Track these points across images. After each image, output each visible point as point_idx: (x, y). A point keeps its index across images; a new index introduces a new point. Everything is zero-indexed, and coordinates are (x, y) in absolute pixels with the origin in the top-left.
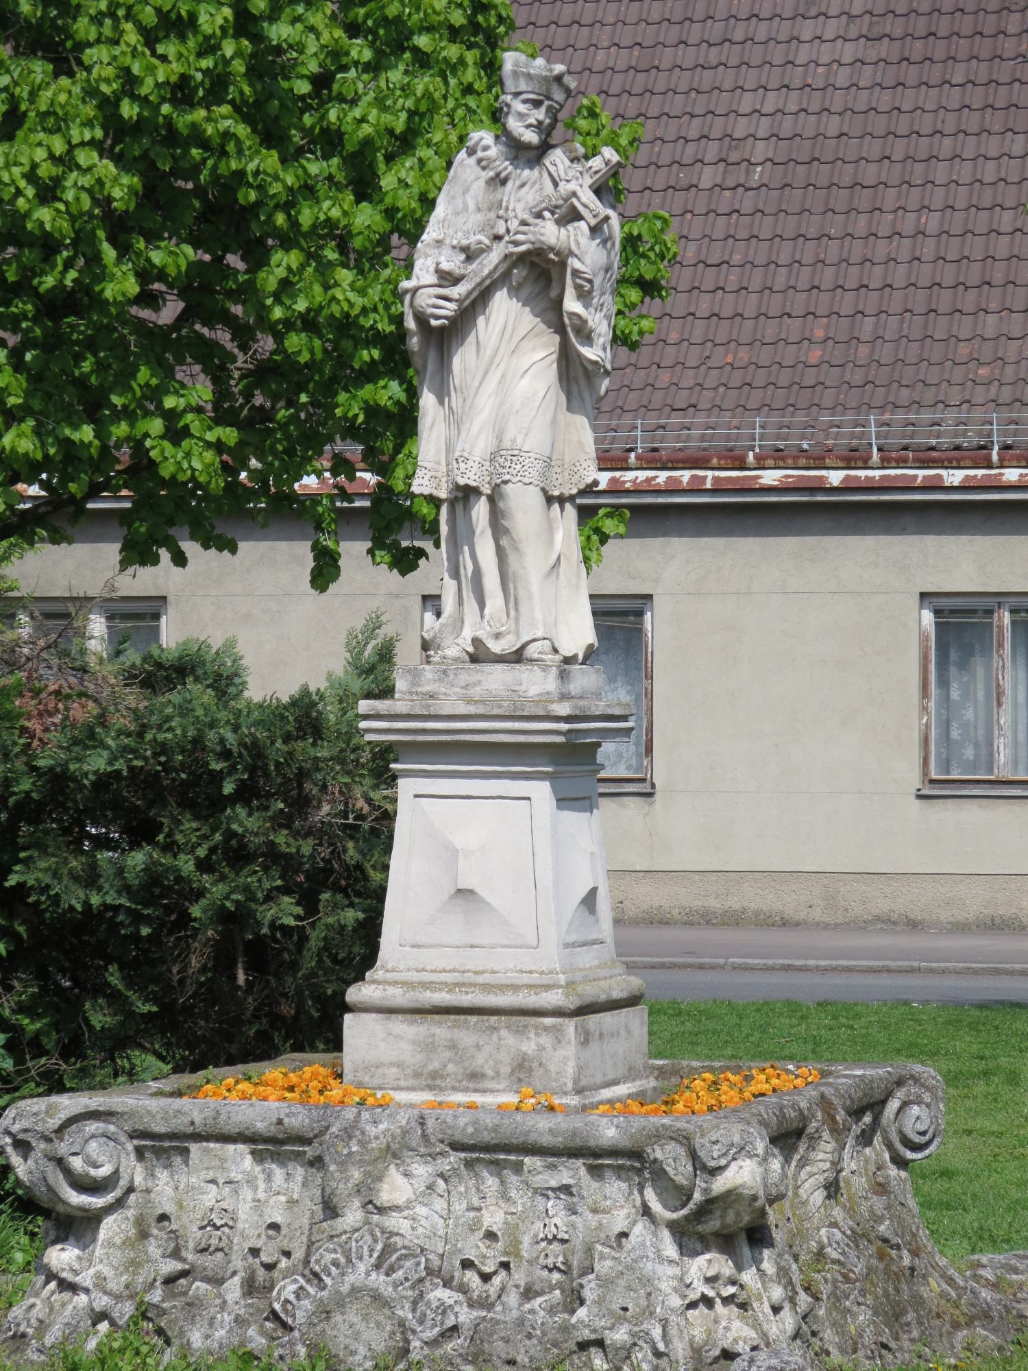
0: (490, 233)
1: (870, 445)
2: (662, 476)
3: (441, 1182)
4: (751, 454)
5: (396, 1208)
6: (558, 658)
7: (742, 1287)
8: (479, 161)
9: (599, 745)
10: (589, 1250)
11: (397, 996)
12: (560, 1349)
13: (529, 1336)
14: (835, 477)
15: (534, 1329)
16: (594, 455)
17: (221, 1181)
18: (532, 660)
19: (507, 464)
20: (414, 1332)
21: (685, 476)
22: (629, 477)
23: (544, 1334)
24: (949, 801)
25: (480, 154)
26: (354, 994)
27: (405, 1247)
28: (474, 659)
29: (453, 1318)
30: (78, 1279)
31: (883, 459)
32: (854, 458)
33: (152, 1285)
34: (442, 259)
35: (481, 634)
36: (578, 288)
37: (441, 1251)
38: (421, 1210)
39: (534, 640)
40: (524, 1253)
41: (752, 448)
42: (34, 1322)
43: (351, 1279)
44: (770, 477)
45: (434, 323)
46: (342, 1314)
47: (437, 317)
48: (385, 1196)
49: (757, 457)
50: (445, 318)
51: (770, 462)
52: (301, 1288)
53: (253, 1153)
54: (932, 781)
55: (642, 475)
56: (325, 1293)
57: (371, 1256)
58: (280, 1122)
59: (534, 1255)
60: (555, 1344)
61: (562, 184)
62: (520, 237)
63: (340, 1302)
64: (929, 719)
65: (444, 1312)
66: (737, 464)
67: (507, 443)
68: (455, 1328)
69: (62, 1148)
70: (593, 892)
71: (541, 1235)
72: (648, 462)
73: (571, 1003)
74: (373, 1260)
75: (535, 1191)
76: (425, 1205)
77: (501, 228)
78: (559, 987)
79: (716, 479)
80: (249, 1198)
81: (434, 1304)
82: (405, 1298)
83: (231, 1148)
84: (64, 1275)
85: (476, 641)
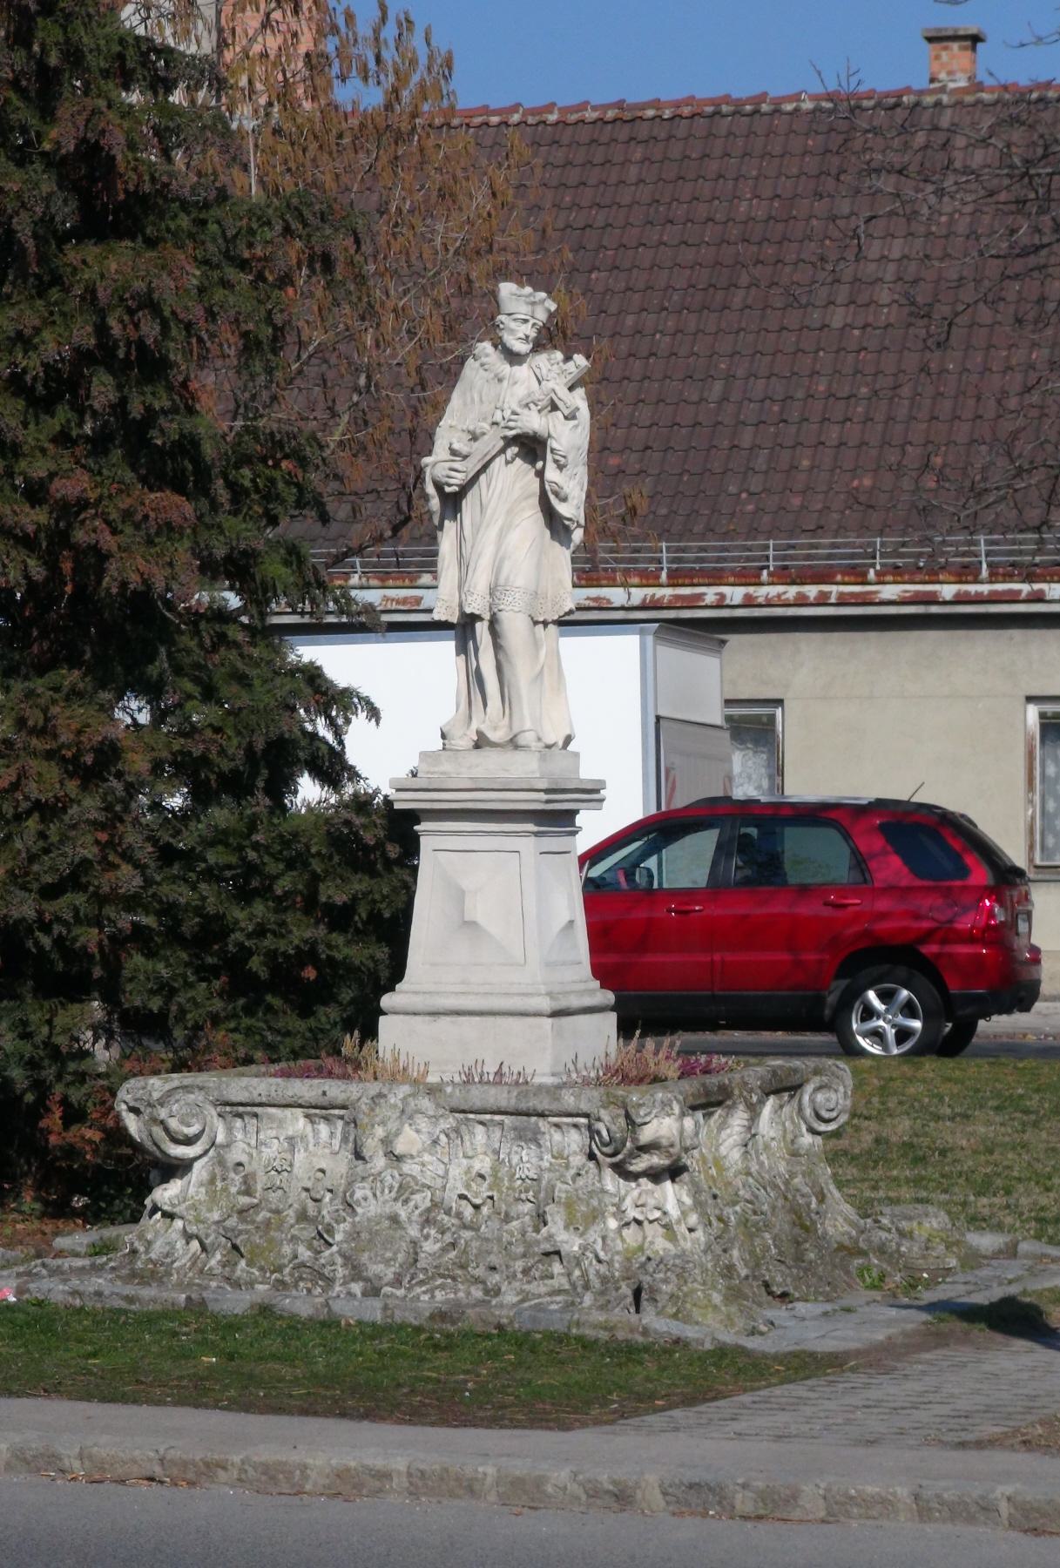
0: (490, 421)
1: (980, 563)
2: (792, 591)
4: (872, 571)
6: (541, 745)
7: (665, 1213)
8: (482, 365)
9: (576, 812)
11: (418, 1002)
21: (812, 591)
22: (762, 592)
24: (1052, 884)
26: (386, 1001)
28: (477, 746)
30: (176, 1210)
31: (991, 575)
34: (454, 440)
35: (483, 728)
41: (873, 565)
44: (890, 591)
45: (448, 489)
47: (450, 485)
48: (400, 1148)
49: (878, 574)
51: (889, 578)
53: (307, 1116)
54: (1037, 867)
55: (773, 591)
61: (543, 383)
62: (511, 424)
64: (1034, 812)
66: (860, 580)
67: (502, 581)
69: (163, 1113)
70: (571, 922)
72: (779, 577)
73: (546, 1004)
77: (498, 417)
78: (540, 995)
79: (841, 595)
83: (288, 1112)
84: (166, 1208)
85: (480, 733)
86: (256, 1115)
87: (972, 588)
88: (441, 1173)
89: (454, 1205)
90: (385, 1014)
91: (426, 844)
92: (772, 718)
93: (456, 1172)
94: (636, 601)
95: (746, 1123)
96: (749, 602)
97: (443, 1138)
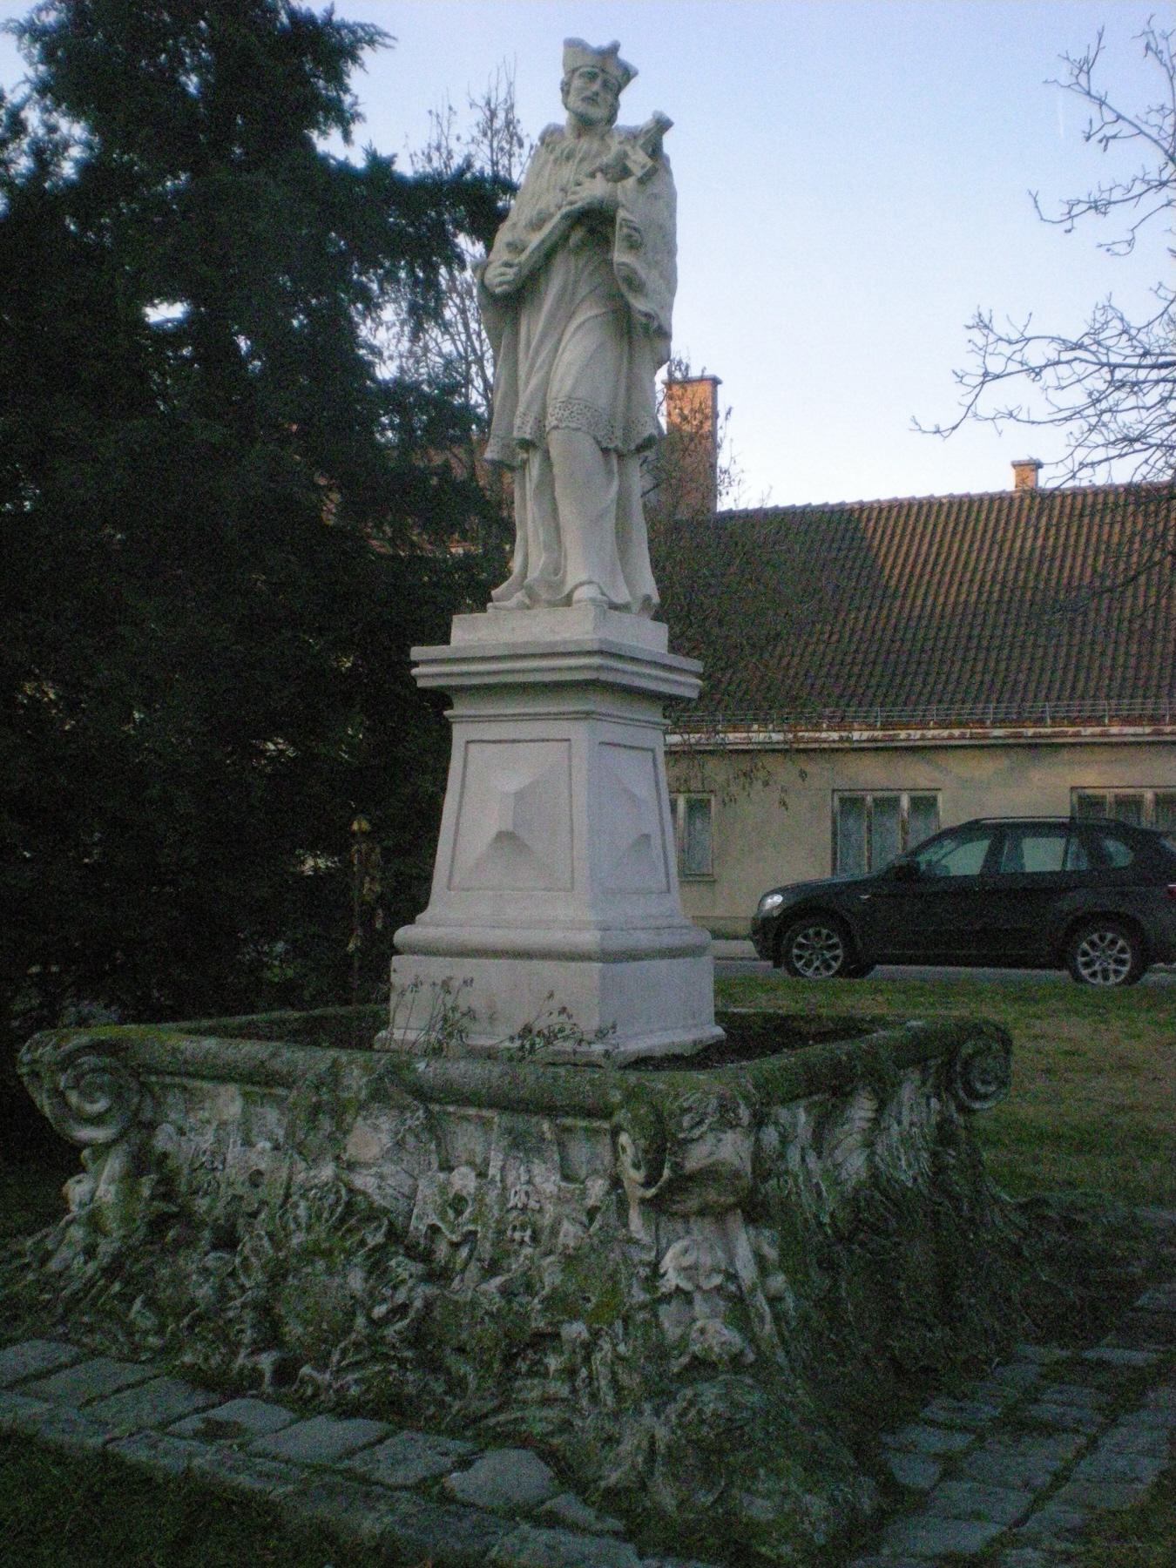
2: (945, 733)
21: (956, 732)
26: (402, 935)
55: (936, 732)
86: (185, 1089)
87: (1042, 730)
88: (406, 1190)
89: (422, 1241)
90: (398, 952)
91: (459, 734)
92: (935, 799)
93: (426, 1190)
94: (864, 738)
95: (870, 1115)
96: (923, 738)
97: (411, 1140)
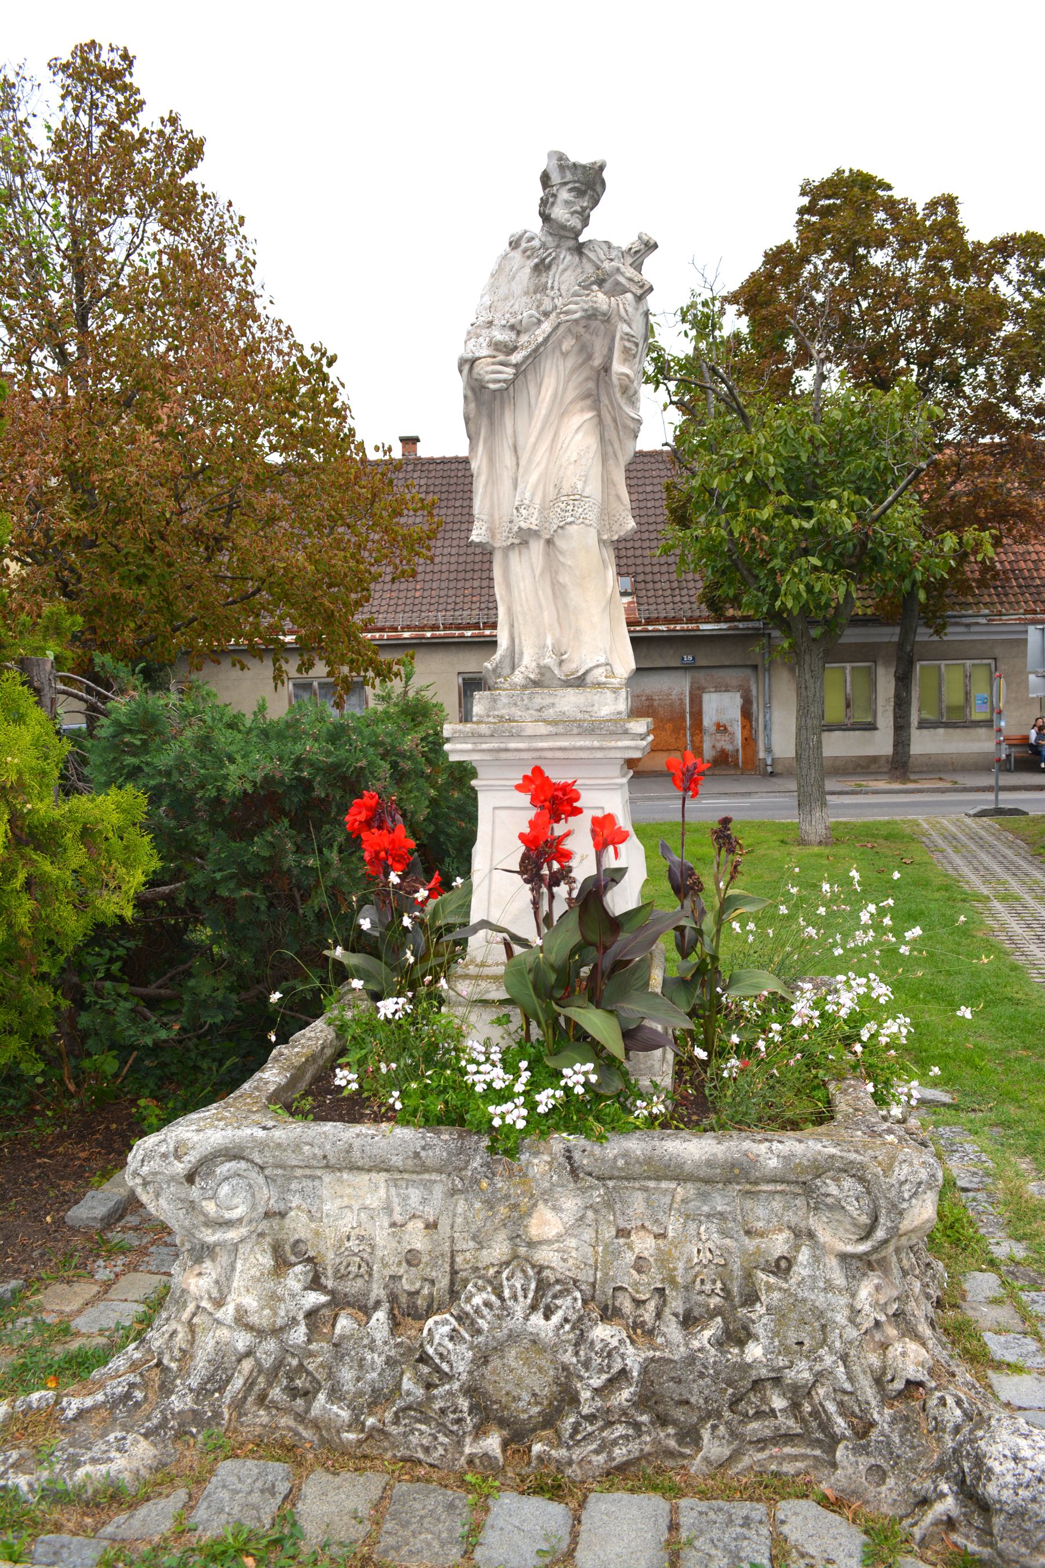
3: (590, 1214)
5: (548, 1242)
10: (748, 1276)
12: (735, 1388)
13: (702, 1375)
14: (429, 634)
15: (706, 1368)
16: (629, 507)
17: (356, 1207)
18: (599, 685)
19: (570, 508)
20: (581, 1378)
23: (717, 1373)
25: (524, 245)
27: (558, 1281)
29: (619, 1360)
32: (434, 628)
33: (294, 1321)
36: (626, 350)
37: (592, 1280)
38: (572, 1242)
39: (598, 666)
40: (679, 1280)
42: (177, 1354)
43: (509, 1324)
44: (406, 635)
45: (492, 386)
46: (502, 1357)
50: (505, 381)
52: (454, 1330)
56: (481, 1339)
57: (525, 1297)
58: (417, 1155)
59: (689, 1280)
60: (730, 1383)
63: (499, 1349)
65: (609, 1355)
67: (566, 489)
68: (624, 1372)
71: (696, 1260)
74: (529, 1301)
75: (688, 1216)
76: (575, 1236)
80: (386, 1224)
81: (598, 1347)
82: (568, 1341)
